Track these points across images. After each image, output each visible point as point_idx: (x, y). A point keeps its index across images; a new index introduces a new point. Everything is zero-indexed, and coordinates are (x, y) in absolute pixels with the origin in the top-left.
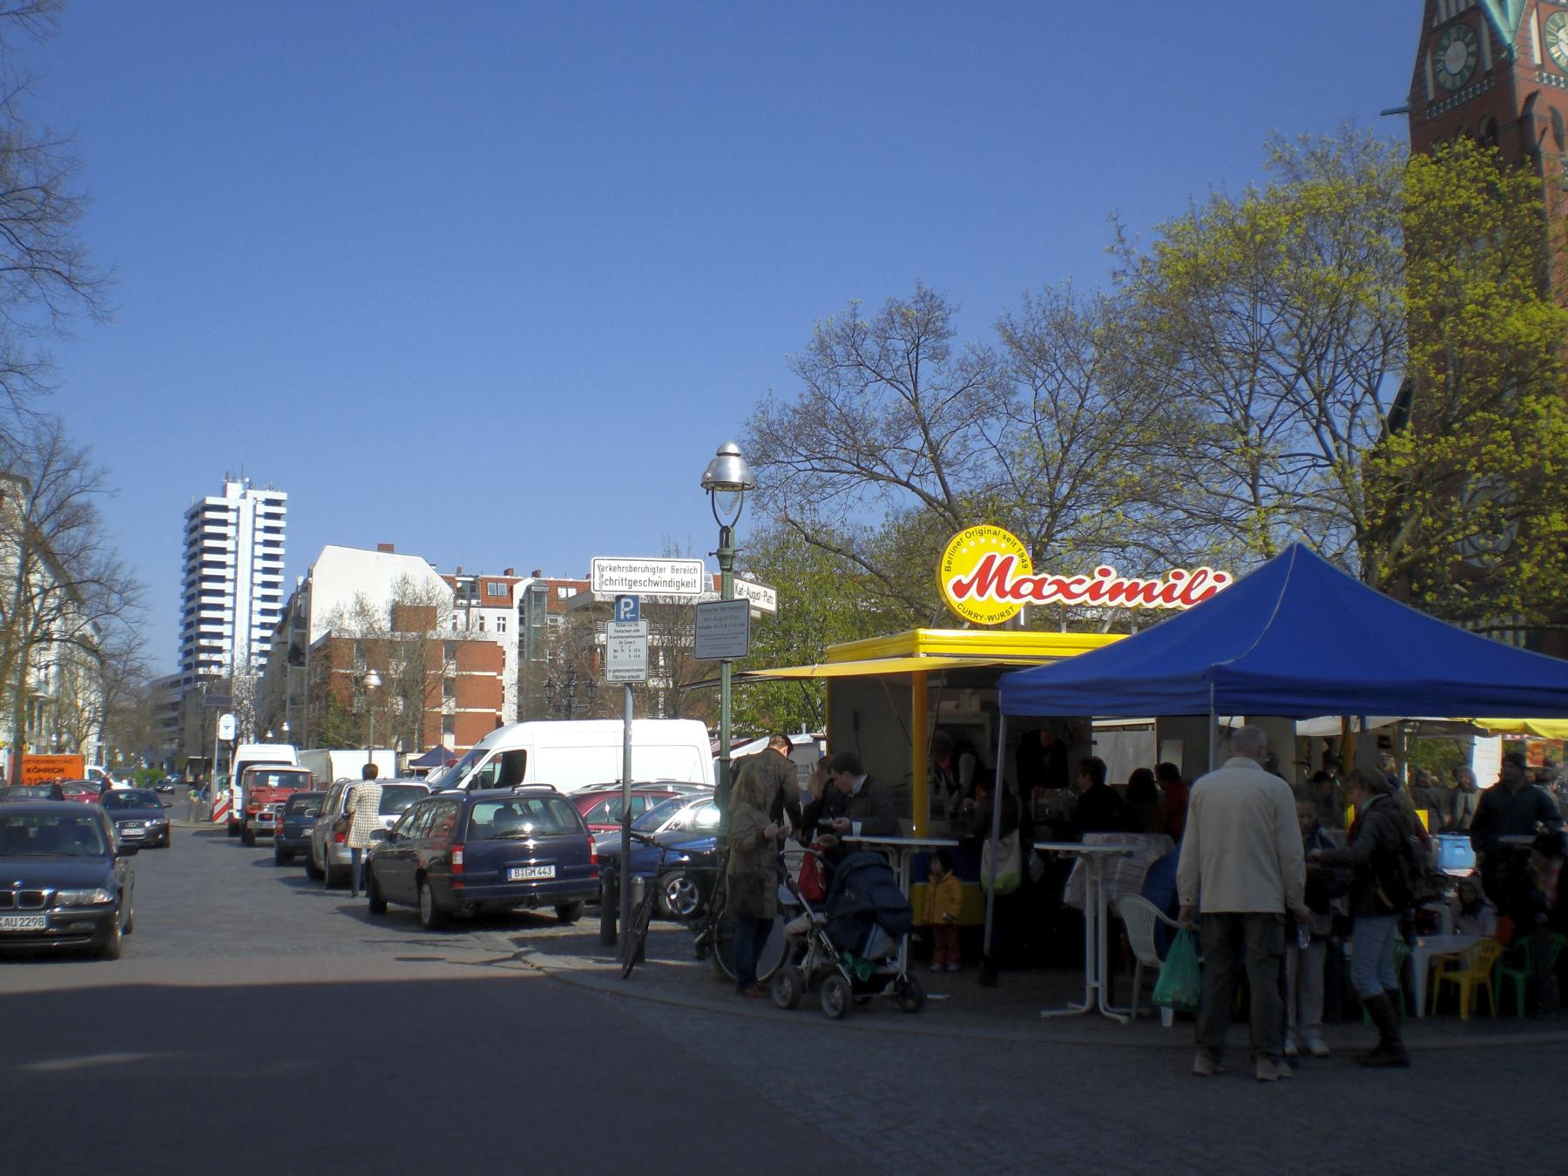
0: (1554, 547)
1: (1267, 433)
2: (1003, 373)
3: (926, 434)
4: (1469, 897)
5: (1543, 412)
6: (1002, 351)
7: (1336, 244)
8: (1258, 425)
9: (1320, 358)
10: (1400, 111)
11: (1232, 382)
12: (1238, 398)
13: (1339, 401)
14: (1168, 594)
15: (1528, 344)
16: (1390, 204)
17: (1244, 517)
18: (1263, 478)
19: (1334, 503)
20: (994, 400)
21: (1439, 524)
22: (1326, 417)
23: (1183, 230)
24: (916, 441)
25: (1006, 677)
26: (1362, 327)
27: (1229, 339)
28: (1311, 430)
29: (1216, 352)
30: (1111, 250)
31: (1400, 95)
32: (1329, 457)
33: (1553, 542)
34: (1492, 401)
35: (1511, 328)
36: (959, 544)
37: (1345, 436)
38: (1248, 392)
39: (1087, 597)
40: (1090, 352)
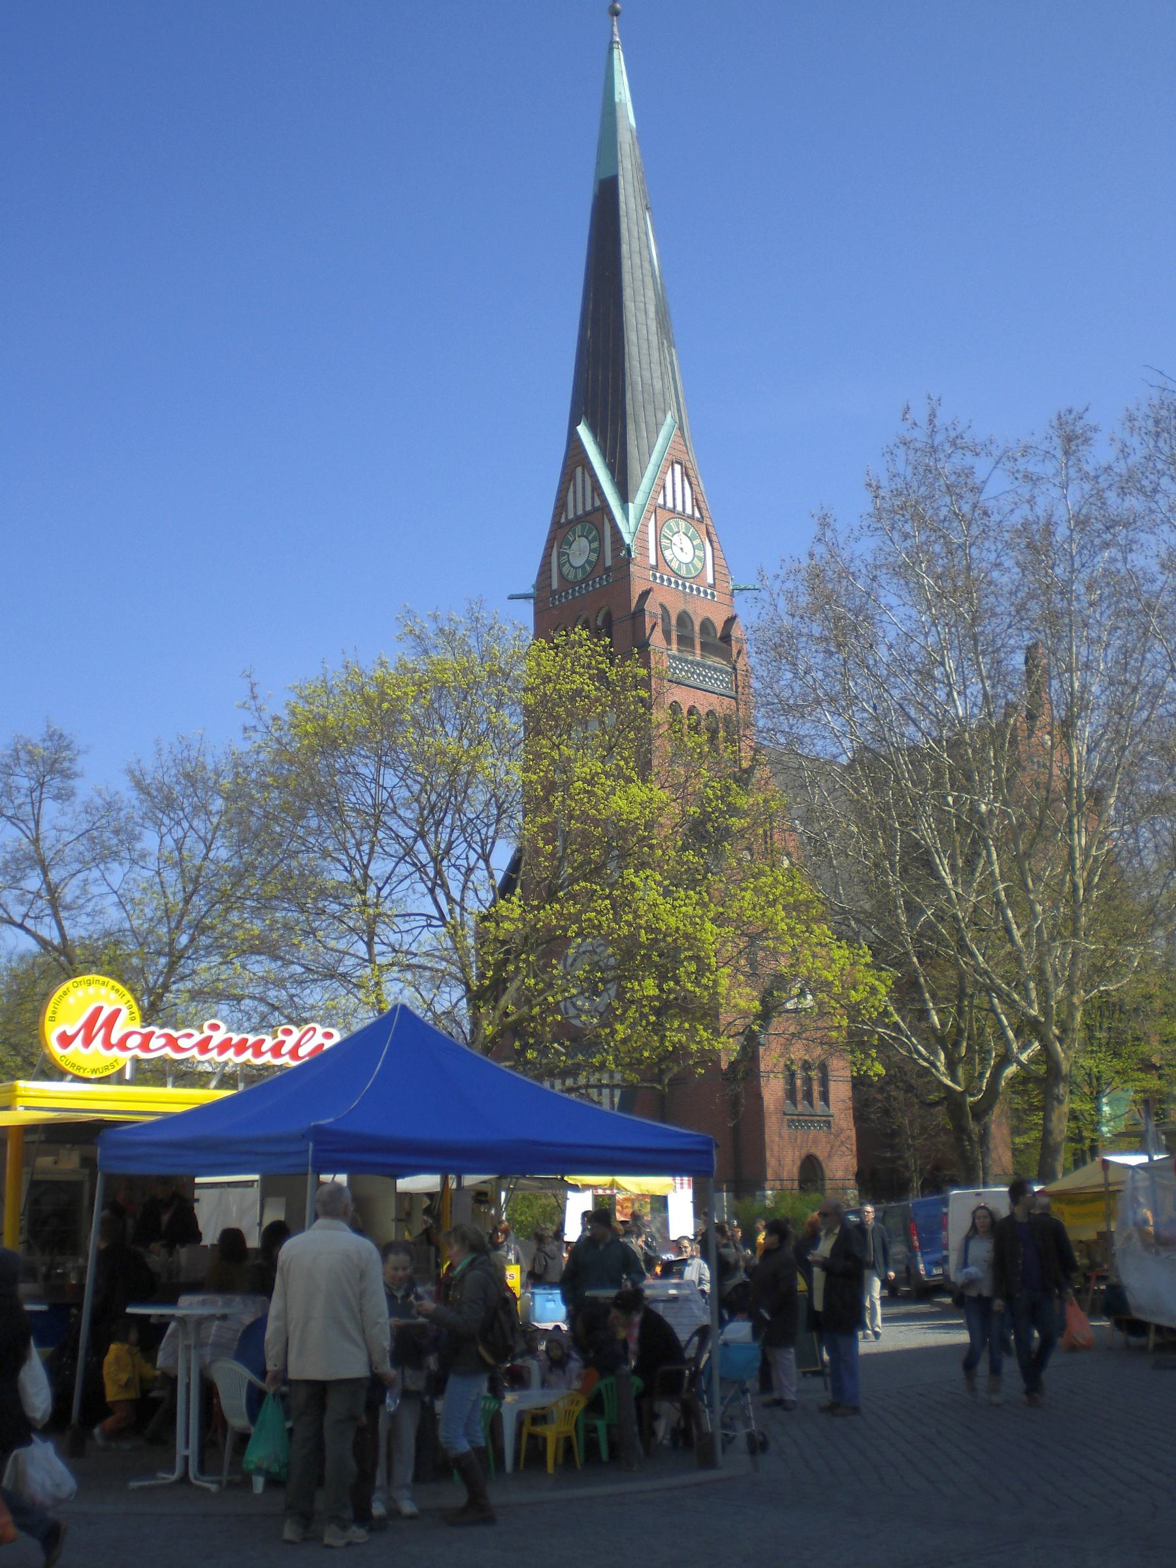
0: (646, 1010)
1: (384, 893)
2: (129, 819)
3: (45, 874)
4: (557, 1353)
5: (641, 885)
6: (129, 796)
7: (458, 716)
8: (376, 885)
9: (439, 823)
10: (526, 597)
11: (353, 841)
12: (358, 857)
13: (454, 865)
14: (276, 1051)
15: (628, 821)
16: (509, 683)
17: (358, 974)
18: (378, 936)
19: (444, 963)
20: (117, 845)
21: (541, 985)
22: (441, 879)
23: (314, 691)
24: (33, 882)
25: (107, 1133)
26: (479, 796)
27: (353, 799)
28: (426, 891)
29: (339, 812)
30: (243, 706)
31: (527, 582)
32: (442, 917)
33: (646, 1006)
34: (595, 872)
35: (614, 806)
36: (65, 993)
37: (458, 899)
38: (367, 851)
39: (195, 1052)
40: (218, 804)
